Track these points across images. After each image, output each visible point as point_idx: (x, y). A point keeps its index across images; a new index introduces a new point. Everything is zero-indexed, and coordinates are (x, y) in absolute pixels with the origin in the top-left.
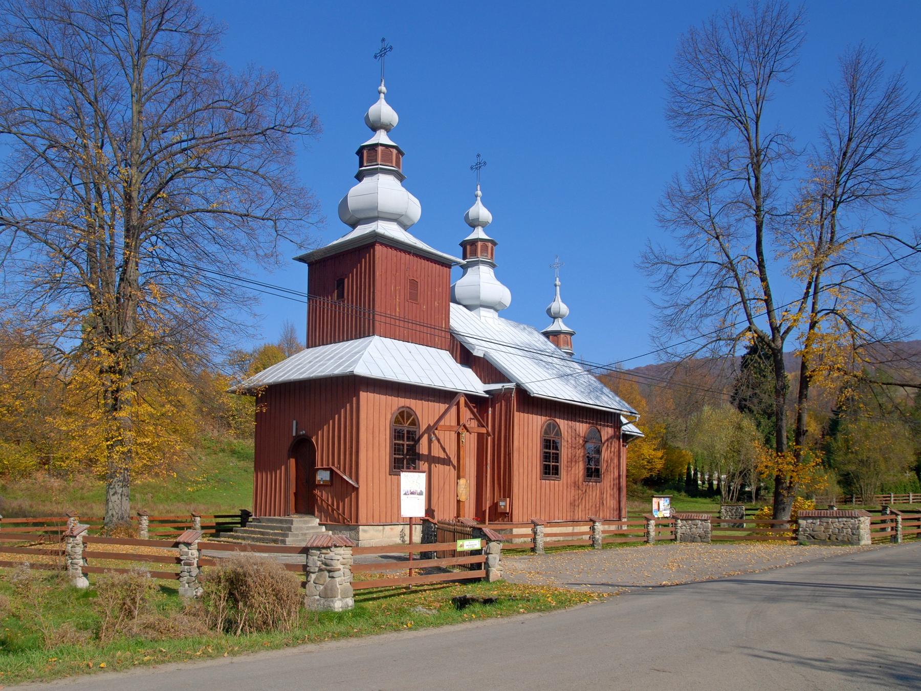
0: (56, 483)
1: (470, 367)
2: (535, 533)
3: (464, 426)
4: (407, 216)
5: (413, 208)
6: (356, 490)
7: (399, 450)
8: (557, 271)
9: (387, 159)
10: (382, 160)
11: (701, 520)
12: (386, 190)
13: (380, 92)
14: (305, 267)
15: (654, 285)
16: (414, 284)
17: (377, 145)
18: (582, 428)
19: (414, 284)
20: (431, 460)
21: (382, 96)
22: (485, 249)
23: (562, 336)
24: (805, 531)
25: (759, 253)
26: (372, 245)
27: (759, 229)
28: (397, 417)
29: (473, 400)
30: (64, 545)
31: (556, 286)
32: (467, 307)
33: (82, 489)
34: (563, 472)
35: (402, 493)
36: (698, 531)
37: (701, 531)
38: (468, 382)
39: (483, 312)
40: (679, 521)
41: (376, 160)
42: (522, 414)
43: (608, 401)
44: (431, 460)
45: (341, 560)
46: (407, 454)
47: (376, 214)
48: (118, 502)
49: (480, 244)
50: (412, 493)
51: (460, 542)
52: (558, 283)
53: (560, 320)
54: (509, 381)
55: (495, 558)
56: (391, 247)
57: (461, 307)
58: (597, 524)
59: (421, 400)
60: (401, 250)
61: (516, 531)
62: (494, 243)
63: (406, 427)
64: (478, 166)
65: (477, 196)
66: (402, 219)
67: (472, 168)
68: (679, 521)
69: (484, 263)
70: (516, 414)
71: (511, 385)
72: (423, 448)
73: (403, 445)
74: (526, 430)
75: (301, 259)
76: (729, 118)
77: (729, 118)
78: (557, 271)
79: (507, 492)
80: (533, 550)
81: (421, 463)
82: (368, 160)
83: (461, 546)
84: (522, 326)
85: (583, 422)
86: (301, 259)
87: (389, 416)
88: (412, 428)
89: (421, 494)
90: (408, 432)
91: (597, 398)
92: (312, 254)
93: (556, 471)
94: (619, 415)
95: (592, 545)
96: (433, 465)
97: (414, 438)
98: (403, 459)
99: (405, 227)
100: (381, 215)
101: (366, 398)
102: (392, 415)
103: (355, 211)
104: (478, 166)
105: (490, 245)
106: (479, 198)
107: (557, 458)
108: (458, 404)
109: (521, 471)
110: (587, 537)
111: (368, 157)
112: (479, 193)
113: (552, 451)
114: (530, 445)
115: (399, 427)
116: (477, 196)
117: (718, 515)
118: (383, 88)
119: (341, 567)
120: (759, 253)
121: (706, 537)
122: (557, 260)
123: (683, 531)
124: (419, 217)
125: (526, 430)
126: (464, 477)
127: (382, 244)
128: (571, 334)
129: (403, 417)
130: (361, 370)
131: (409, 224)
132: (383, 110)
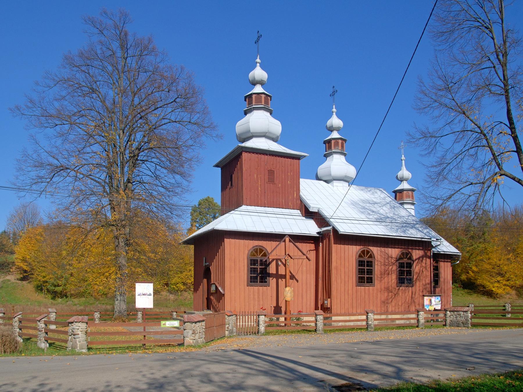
0: (172, 297)
1: (313, 219)
2: (316, 320)
3: (288, 255)
4: (270, 133)
5: (275, 126)
6: (224, 295)
7: (362, 272)
8: (402, 151)
9: (259, 101)
10: (255, 103)
11: (463, 312)
12: (259, 120)
13: (257, 63)
14: (219, 169)
15: (423, 153)
16: (271, 173)
17: (251, 94)
18: (394, 252)
19: (271, 173)
20: (278, 276)
21: (258, 64)
22: (337, 144)
23: (405, 192)
25: (510, 119)
26: (241, 154)
27: (508, 102)
30: (67, 328)
31: (402, 160)
32: (327, 182)
33: (185, 300)
34: (376, 282)
35: (137, 294)
37: (463, 319)
38: (311, 228)
39: (335, 183)
40: (448, 312)
41: (261, 103)
42: (339, 246)
44: (278, 276)
46: (260, 273)
47: (250, 135)
48: (119, 304)
49: (333, 142)
50: (144, 295)
51: (163, 322)
52: (403, 158)
53: (405, 182)
54: (330, 226)
56: (253, 153)
57: (322, 182)
58: (370, 314)
59: (270, 241)
60: (260, 154)
61: (334, 318)
62: (345, 141)
63: (366, 259)
64: (333, 94)
65: (333, 112)
68: (448, 312)
70: (333, 245)
71: (329, 228)
72: (272, 269)
73: (257, 268)
74: (343, 255)
75: (217, 166)
76: (478, 27)
77: (478, 27)
78: (402, 151)
79: (329, 296)
80: (316, 330)
81: (271, 279)
82: (251, 103)
83: (164, 324)
84: (369, 189)
85: (395, 248)
86: (217, 166)
87: (246, 252)
88: (370, 259)
89: (150, 295)
90: (368, 262)
91: (404, 232)
92: (220, 162)
93: (370, 281)
95: (367, 328)
96: (280, 280)
97: (266, 264)
98: (257, 277)
99: (275, 140)
100: (254, 135)
101: (228, 242)
102: (249, 251)
104: (333, 94)
105: (340, 141)
106: (334, 113)
107: (370, 272)
108: (285, 241)
109: (339, 281)
110: (364, 323)
112: (334, 110)
114: (347, 264)
115: (361, 259)
116: (333, 112)
117: (504, 308)
118: (258, 60)
119: (80, 333)
120: (510, 119)
121: (467, 323)
122: (402, 144)
124: (280, 131)
125: (343, 255)
126: (289, 286)
127: (246, 152)
128: (413, 190)
129: (256, 252)
131: (274, 137)
132: (259, 73)
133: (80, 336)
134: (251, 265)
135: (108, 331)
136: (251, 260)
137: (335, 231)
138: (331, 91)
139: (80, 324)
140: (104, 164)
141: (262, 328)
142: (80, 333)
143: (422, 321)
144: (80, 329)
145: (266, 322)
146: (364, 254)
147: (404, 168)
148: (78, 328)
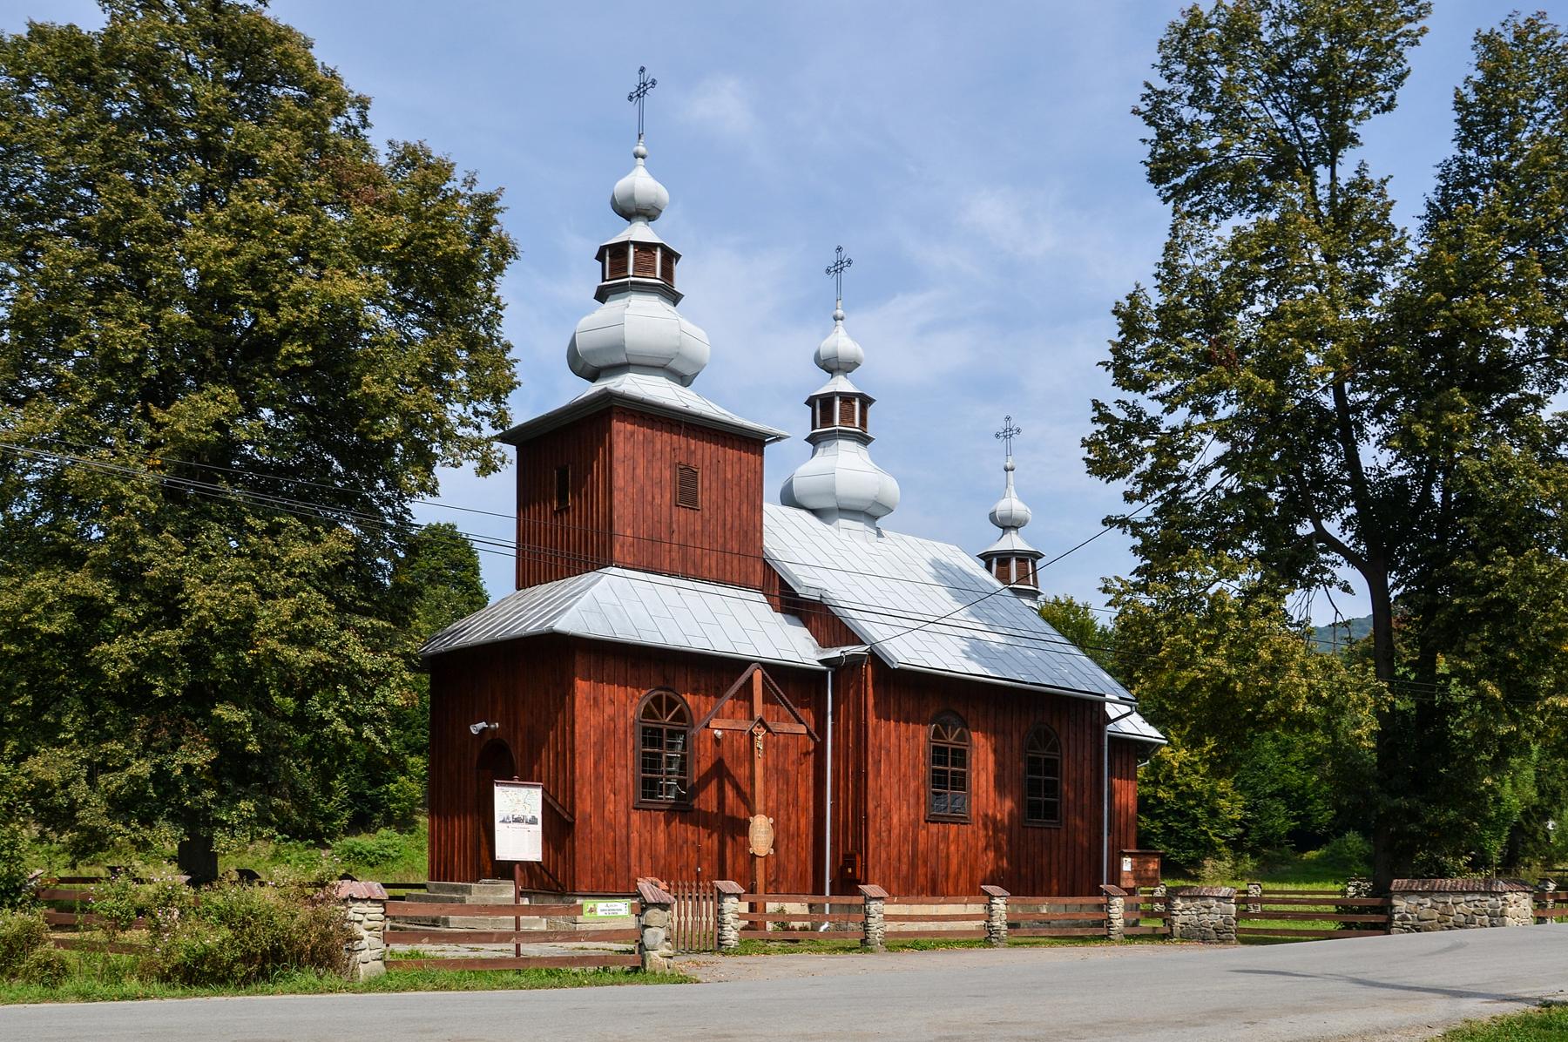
1: (806, 624)
11: (1219, 899)
17: (626, 244)
24: (1404, 918)
28: (647, 706)
29: (783, 676)
32: (815, 512)
36: (1213, 919)
38: (798, 647)
41: (626, 269)
43: (1076, 672)
45: (366, 923)
47: (623, 359)
50: (517, 820)
54: (862, 643)
55: (656, 935)
57: (803, 513)
66: (672, 365)
67: (828, 271)
69: (845, 435)
83: (591, 911)
89: (533, 821)
94: (1101, 704)
100: (632, 360)
103: (586, 353)
107: (1052, 788)
111: (635, 259)
113: (950, 768)
115: (651, 723)
119: (365, 934)
123: (1185, 919)
130: (566, 624)
133: (364, 943)
134: (644, 746)
135: (481, 928)
136: (645, 730)
137: (876, 659)
138: (831, 259)
139: (364, 908)
140: (1210, 577)
141: (731, 936)
142: (365, 934)
143: (999, 923)
144: (366, 923)
145: (741, 916)
146: (660, 708)
147: (1013, 494)
148: (359, 917)
